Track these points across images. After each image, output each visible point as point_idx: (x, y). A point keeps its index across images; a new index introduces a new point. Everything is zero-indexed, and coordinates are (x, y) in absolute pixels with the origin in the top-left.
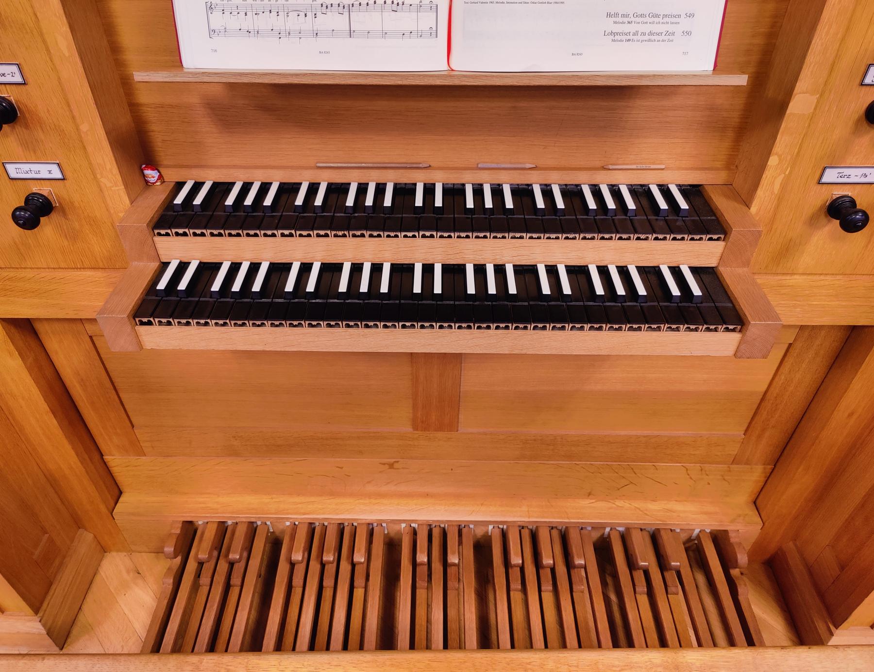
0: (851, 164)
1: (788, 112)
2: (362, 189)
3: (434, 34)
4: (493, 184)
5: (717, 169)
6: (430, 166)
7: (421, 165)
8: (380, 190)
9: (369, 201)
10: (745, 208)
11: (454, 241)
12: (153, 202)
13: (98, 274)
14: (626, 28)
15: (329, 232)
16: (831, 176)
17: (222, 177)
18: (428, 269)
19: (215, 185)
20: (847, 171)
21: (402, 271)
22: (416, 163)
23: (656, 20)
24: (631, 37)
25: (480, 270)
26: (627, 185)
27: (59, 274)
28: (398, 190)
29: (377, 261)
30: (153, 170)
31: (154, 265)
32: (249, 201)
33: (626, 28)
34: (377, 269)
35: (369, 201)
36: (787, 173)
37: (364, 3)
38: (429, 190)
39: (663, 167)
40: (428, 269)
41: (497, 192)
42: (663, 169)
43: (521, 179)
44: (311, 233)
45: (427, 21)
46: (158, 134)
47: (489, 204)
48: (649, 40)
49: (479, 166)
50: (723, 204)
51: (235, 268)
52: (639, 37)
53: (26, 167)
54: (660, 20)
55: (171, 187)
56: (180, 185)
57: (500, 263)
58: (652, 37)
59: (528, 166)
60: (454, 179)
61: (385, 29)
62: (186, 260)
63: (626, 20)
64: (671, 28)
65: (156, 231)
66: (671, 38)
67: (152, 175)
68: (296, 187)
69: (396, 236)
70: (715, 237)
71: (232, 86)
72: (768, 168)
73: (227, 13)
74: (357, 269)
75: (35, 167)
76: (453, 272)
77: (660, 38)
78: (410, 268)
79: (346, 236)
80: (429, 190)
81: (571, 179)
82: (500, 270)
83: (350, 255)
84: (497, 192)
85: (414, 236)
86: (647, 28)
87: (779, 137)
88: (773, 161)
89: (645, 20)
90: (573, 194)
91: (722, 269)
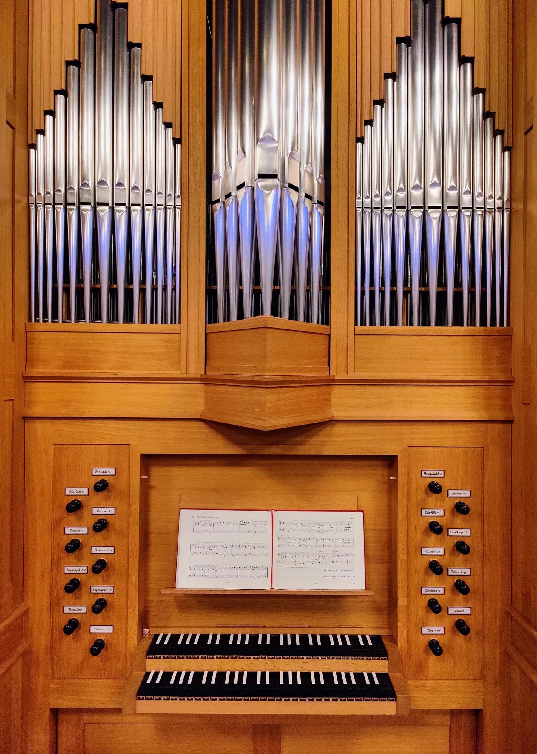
0: (431, 625)
1: (398, 604)
2: (236, 637)
3: (266, 577)
4: (292, 635)
5: (385, 628)
6: (265, 626)
7: (261, 626)
8: (243, 637)
9: (239, 642)
10: (395, 645)
11: (275, 660)
12: (147, 643)
13: (110, 681)
14: (332, 575)
15: (221, 656)
16: (425, 631)
17: (175, 631)
18: (263, 674)
19: (172, 636)
20: (431, 629)
21: (252, 675)
22: (259, 625)
23: (342, 572)
24: (334, 578)
25: (286, 675)
26: (349, 635)
27: (91, 681)
28: (251, 637)
29: (241, 671)
30: (147, 629)
31: (143, 673)
32: (188, 642)
33: (332, 575)
34: (241, 674)
35: (239, 642)
36: (407, 629)
37: (243, 567)
38: (264, 637)
39: (362, 627)
40: (263, 674)
41: (293, 638)
42: (362, 628)
43: (304, 632)
44: (214, 656)
45: (264, 572)
46: (153, 612)
47: (289, 643)
48: (340, 579)
49: (286, 626)
50: (387, 644)
51: (179, 674)
52: (337, 578)
53: (98, 627)
54: (343, 572)
55: (153, 637)
56: (156, 636)
57: (295, 671)
58: (342, 578)
59: (306, 626)
60: (275, 632)
61: (250, 575)
62: (180, 671)
63: (331, 572)
64: (347, 575)
65: (148, 656)
66: (348, 578)
67: (146, 630)
68: (178, 636)
69: (250, 658)
70: (384, 658)
71: (188, 595)
72: (398, 627)
73: (196, 569)
74: (232, 674)
75: (102, 627)
76: (275, 676)
77: (344, 578)
78: (278, 674)
79: (356, 659)
80: (264, 637)
81: (325, 632)
82: (294, 675)
83: (238, 668)
84: (293, 638)
85: (258, 658)
86: (339, 575)
87: (398, 614)
88: (399, 624)
89: (338, 572)
90: (325, 638)
91: (389, 674)
